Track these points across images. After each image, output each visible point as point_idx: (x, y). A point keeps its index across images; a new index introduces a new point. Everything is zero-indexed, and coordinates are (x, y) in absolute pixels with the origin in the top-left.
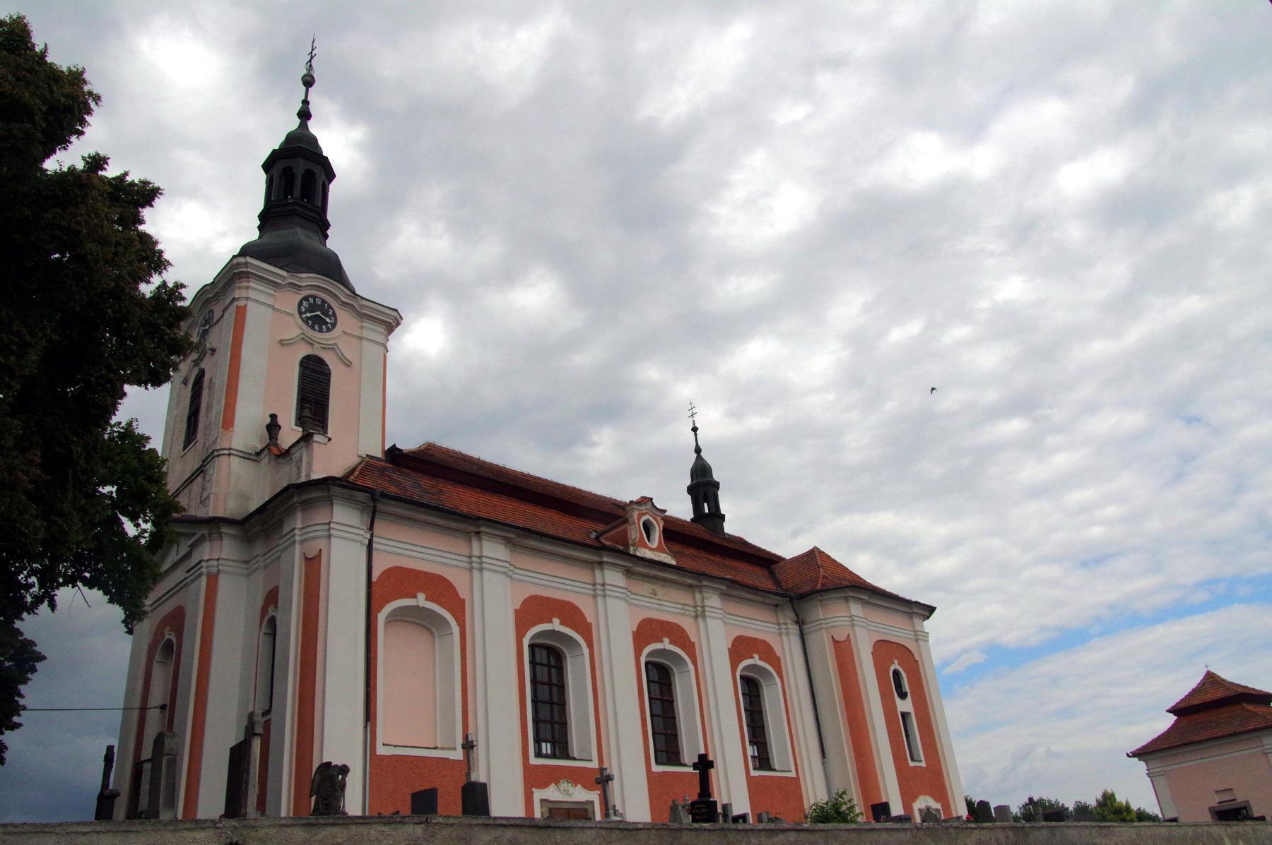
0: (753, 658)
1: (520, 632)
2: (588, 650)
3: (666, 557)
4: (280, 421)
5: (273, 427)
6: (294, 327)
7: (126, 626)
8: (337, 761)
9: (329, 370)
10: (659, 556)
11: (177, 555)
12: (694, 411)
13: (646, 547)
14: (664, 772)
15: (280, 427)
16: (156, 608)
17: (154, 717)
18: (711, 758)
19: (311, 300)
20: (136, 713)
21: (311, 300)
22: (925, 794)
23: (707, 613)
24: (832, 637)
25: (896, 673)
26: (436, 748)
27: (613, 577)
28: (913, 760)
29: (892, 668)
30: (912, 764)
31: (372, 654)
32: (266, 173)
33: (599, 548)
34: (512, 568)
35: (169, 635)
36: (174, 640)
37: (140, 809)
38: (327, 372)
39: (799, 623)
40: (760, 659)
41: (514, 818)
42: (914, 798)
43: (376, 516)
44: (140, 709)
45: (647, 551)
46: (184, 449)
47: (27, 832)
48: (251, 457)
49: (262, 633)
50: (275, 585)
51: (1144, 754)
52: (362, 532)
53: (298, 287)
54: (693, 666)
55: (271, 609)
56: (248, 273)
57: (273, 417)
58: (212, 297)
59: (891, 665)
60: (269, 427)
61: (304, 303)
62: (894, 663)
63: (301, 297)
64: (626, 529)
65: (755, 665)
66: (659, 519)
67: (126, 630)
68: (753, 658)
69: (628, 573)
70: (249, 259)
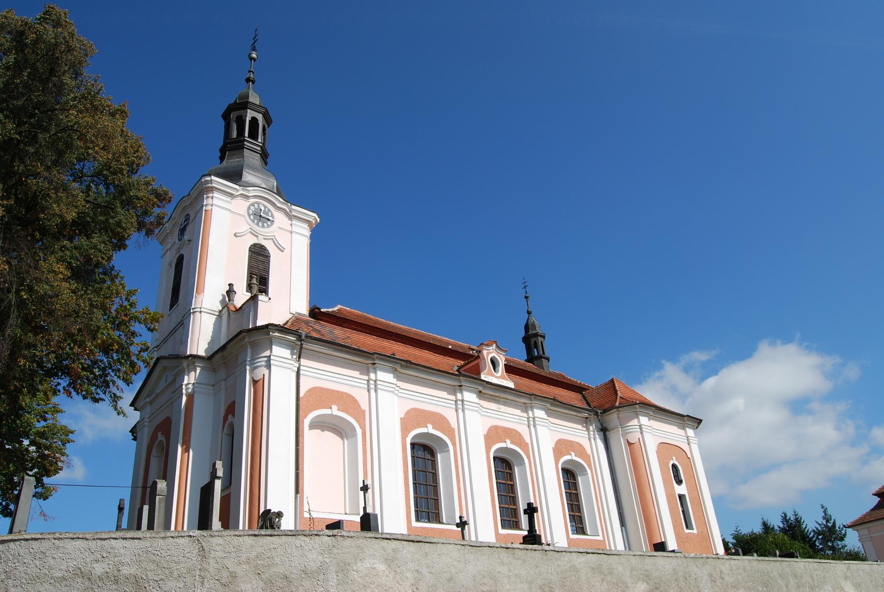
1: (405, 431)
3: (507, 383)
4: (235, 288)
5: (230, 292)
6: (245, 225)
7: (133, 435)
8: (274, 509)
9: (269, 253)
10: (502, 382)
12: (526, 284)
13: (493, 375)
14: (508, 534)
16: (159, 349)
19: (256, 205)
20: (140, 490)
21: (256, 205)
23: (272, 362)
24: (627, 440)
25: (674, 466)
26: (346, 514)
27: (470, 396)
28: (687, 528)
30: (687, 531)
32: (225, 121)
33: (459, 373)
34: (398, 388)
35: (161, 437)
36: (164, 440)
38: (267, 255)
39: (603, 431)
41: (395, 534)
44: (142, 487)
45: (494, 378)
46: (170, 310)
47: (68, 538)
50: (233, 400)
51: (857, 525)
52: (293, 362)
53: (247, 197)
56: (213, 187)
58: (189, 205)
60: (228, 292)
61: (252, 207)
63: (249, 203)
64: (478, 363)
65: (572, 460)
67: (133, 438)
69: (480, 394)
70: (213, 178)
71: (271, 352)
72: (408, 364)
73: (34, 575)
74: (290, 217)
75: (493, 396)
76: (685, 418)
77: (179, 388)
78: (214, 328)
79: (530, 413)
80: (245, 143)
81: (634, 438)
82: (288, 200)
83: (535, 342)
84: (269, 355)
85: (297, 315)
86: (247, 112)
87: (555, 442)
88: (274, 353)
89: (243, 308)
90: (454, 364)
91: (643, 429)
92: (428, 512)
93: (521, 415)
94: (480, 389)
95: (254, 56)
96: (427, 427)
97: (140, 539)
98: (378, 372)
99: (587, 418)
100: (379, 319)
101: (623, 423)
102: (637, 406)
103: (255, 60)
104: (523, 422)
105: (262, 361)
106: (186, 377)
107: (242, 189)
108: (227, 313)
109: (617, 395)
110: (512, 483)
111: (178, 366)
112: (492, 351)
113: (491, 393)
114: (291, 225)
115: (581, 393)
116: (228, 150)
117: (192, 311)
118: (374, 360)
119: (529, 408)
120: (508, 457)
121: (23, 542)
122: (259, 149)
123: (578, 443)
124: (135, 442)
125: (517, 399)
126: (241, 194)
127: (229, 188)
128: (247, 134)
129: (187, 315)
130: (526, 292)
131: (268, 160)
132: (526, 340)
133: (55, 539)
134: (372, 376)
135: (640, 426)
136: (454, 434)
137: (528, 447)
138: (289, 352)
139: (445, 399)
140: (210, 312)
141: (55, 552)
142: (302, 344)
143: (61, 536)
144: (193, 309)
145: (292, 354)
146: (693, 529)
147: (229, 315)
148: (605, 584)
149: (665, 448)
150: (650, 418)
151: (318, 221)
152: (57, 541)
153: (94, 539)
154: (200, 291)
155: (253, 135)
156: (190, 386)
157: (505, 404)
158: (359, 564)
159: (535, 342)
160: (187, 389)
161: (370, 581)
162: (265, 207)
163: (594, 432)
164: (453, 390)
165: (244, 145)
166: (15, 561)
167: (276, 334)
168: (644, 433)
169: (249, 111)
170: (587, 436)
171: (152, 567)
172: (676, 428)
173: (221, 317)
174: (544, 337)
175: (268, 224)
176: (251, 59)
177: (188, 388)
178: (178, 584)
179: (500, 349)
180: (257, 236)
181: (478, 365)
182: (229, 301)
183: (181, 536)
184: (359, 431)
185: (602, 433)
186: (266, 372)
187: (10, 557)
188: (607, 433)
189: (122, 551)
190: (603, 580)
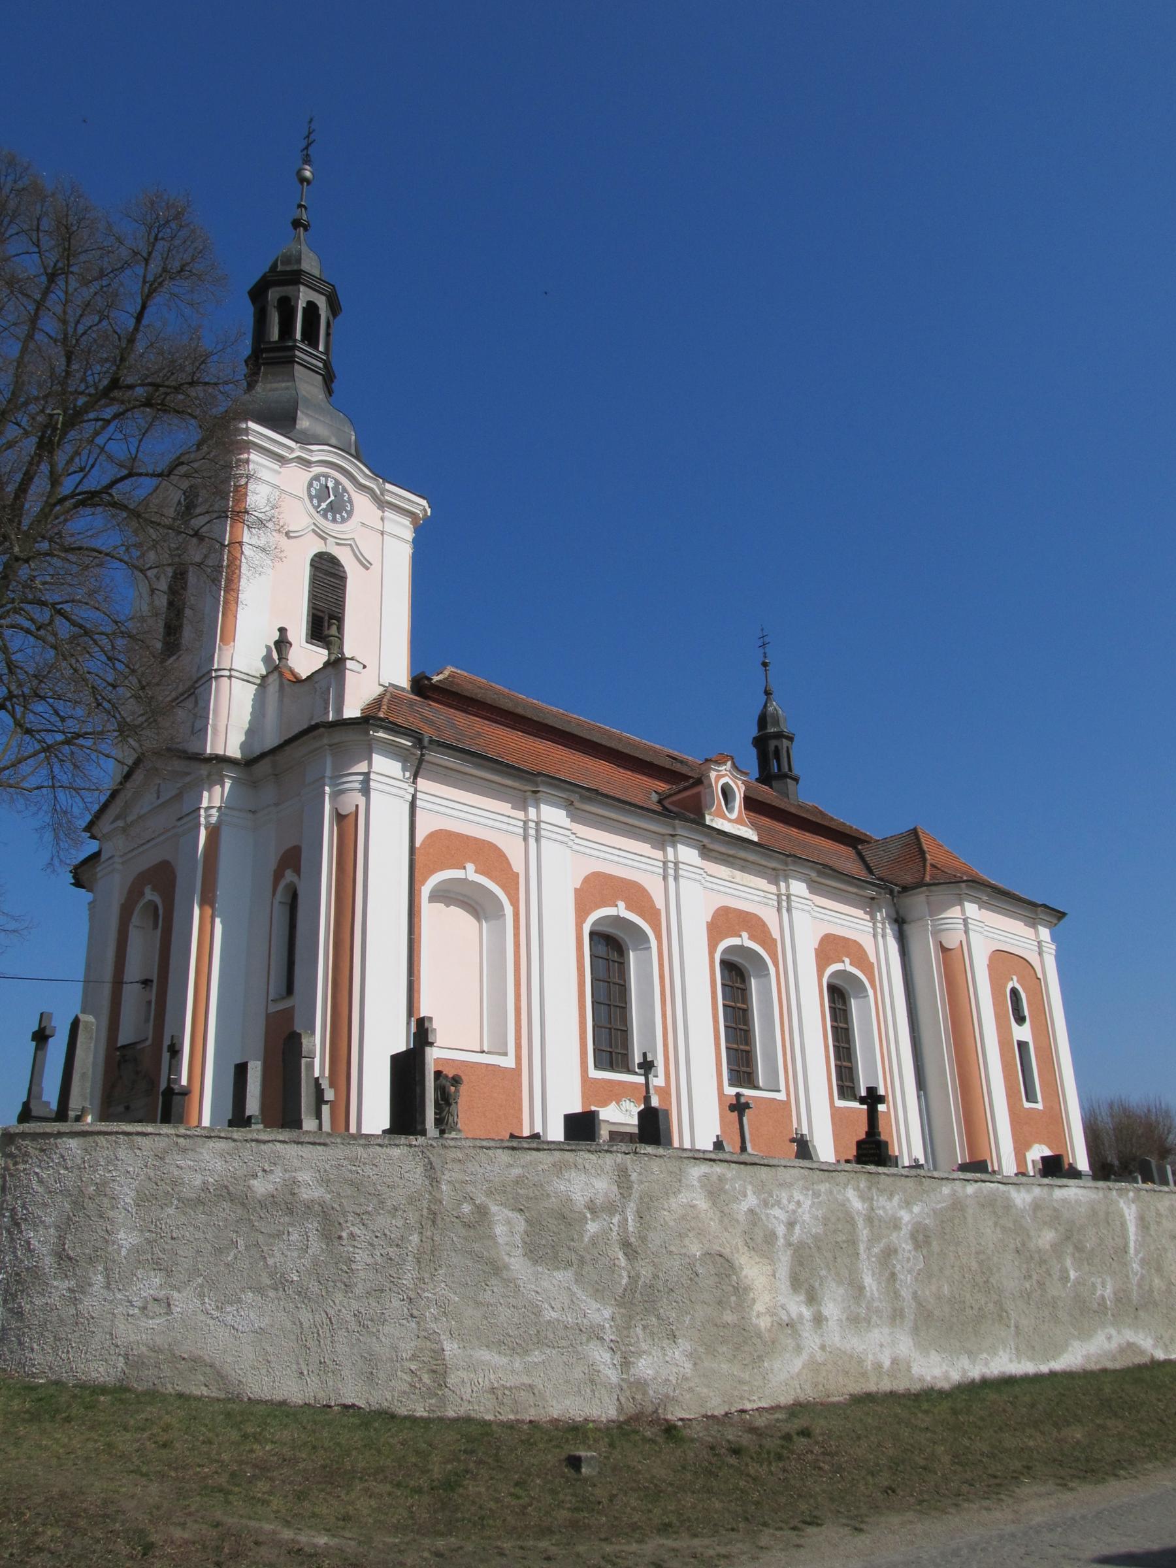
0: (740, 936)
1: (581, 913)
2: (511, 908)
4: (291, 636)
5: (282, 643)
9: (345, 572)
11: (158, 798)
12: (767, 639)
13: (724, 817)
15: (291, 644)
17: (132, 994)
18: (881, 1092)
19: (323, 479)
21: (323, 479)
22: (1040, 1142)
23: (372, 784)
25: (1014, 992)
26: (483, 1052)
27: (687, 854)
29: (1010, 985)
30: (1027, 1105)
31: (415, 937)
37: (248, 1113)
38: (342, 574)
40: (851, 964)
42: (1028, 1146)
43: (423, 766)
45: (725, 822)
48: (251, 679)
49: (276, 903)
52: (405, 786)
53: (307, 463)
54: (511, 908)
55: (289, 876)
57: (282, 630)
59: (1008, 981)
61: (315, 483)
62: (1012, 979)
63: (311, 475)
64: (699, 793)
65: (742, 947)
66: (740, 783)
67: (73, 881)
68: (740, 936)
69: (706, 853)
70: (251, 425)
71: (370, 765)
72: (594, 795)
73: (147, 1192)
74: (382, 504)
75: (724, 854)
76: (1040, 909)
77: (194, 811)
78: (253, 706)
79: (783, 885)
80: (297, 353)
81: (951, 942)
82: (380, 473)
83: (776, 747)
84: (366, 771)
85: (391, 689)
86: (299, 291)
87: (819, 939)
88: (375, 768)
89: (316, 678)
90: (649, 789)
91: (970, 926)
92: (611, 1052)
93: (766, 889)
94: (706, 841)
95: (308, 174)
96: (616, 906)
97: (325, 1144)
98: (543, 807)
99: (873, 899)
100: (517, 694)
101: (936, 909)
102: (963, 885)
103: (308, 181)
104: (771, 902)
105: (355, 782)
106: (206, 794)
107: (300, 447)
108: (277, 682)
109: (924, 860)
110: (744, 1006)
111: (189, 774)
112: (724, 773)
113: (723, 849)
114: (382, 519)
115: (855, 848)
116: (264, 364)
117: (214, 674)
118: (537, 786)
119: (781, 878)
120: (740, 961)
121: (121, 1136)
122: (321, 365)
123: (855, 941)
124: (84, 896)
125: (763, 862)
126: (298, 458)
127: (277, 445)
128: (298, 336)
129: (204, 680)
130: (765, 653)
131: (333, 385)
132: (761, 743)
133: (178, 1136)
134: (532, 812)
135: (964, 920)
136: (659, 920)
137: (776, 945)
138: (399, 765)
139: (649, 858)
140: (246, 677)
141: (179, 1157)
142: (422, 755)
143: (188, 1132)
144: (216, 670)
145: (404, 770)
146: (1037, 1102)
147: (281, 686)
148: (998, 1230)
149: (1003, 961)
150: (983, 905)
151: (429, 514)
152: (181, 1140)
153: (246, 1140)
154: (229, 637)
155: (310, 336)
156: (214, 812)
157: (743, 869)
158: (672, 1200)
159: (776, 747)
160: (208, 816)
161: (688, 1226)
162: (337, 483)
163: (883, 924)
164: (661, 842)
165: (295, 356)
166: (111, 1168)
167: (381, 734)
168: (971, 933)
169: (302, 288)
170: (871, 930)
171: (349, 1192)
172: (1022, 924)
173: (265, 687)
174: (791, 739)
175: (342, 517)
176: (303, 180)
177: (210, 816)
178: (394, 1221)
179: (740, 771)
180: (324, 539)
181: (698, 797)
182: (279, 659)
183: (395, 1145)
184: (508, 910)
185: (896, 927)
186: (361, 801)
187: (101, 1160)
188: (906, 927)
189: (296, 1163)
190: (996, 1224)
